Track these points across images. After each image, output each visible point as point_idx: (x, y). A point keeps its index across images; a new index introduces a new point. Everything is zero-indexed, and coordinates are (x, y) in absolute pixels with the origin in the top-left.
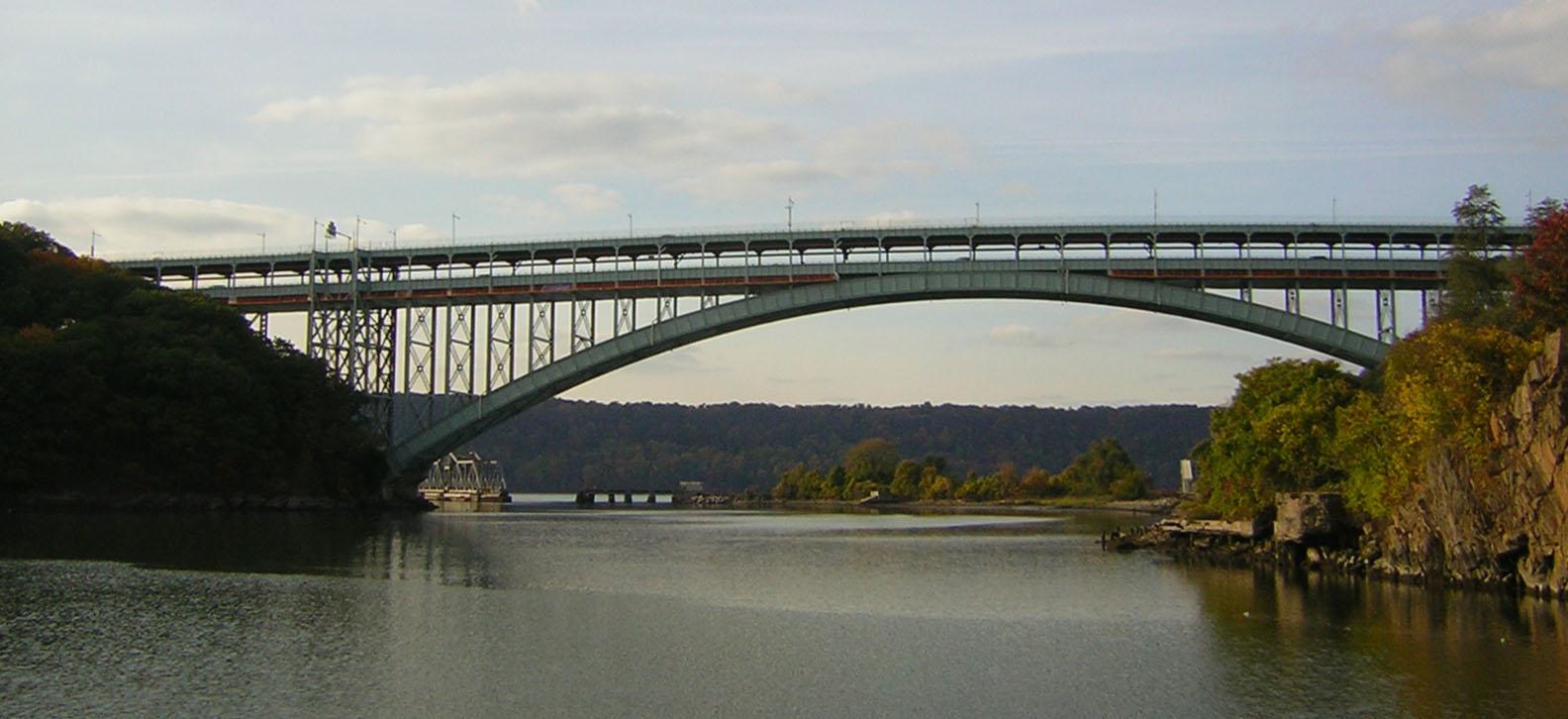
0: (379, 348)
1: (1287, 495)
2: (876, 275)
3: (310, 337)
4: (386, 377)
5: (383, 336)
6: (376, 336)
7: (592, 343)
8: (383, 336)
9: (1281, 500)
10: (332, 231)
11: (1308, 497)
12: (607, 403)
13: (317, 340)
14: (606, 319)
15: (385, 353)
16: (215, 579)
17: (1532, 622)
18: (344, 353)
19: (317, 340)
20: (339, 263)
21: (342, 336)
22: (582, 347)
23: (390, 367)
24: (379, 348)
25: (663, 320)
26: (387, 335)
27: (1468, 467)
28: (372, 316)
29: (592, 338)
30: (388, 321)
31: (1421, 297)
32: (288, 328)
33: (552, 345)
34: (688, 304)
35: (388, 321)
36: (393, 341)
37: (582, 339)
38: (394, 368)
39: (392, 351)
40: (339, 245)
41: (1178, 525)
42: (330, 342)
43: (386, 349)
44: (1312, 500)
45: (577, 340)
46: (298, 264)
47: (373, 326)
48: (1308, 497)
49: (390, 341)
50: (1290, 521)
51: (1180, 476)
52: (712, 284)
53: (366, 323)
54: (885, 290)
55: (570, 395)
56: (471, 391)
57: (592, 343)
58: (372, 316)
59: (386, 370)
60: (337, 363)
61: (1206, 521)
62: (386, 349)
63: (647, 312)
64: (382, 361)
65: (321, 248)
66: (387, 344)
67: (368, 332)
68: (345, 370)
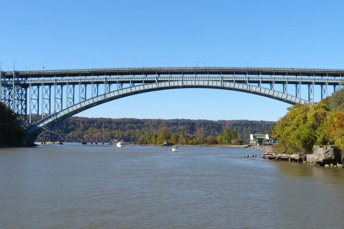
0: (22, 100)
1: (318, 146)
2: (168, 81)
4: (24, 109)
5: (23, 97)
6: (21, 97)
7: (86, 99)
8: (23, 97)
9: (316, 148)
11: (327, 147)
15: (24, 102)
18: (11, 102)
21: (23, 111)
23: (25, 106)
24: (22, 100)
26: (24, 97)
28: (20, 91)
29: (85, 98)
30: (24, 93)
31: (65, 110)
33: (74, 100)
35: (24, 93)
36: (26, 98)
38: (27, 106)
39: (26, 101)
41: (271, 155)
42: (7, 98)
43: (24, 101)
44: (328, 148)
47: (20, 94)
48: (327, 147)
49: (25, 99)
50: (319, 155)
51: (250, 139)
54: (145, 88)
55: (80, 115)
56: (38, 113)
57: (86, 99)
58: (20, 91)
59: (24, 107)
60: (9, 105)
61: (281, 154)
62: (24, 101)
64: (23, 104)
66: (24, 99)
67: (18, 96)
68: (11, 107)
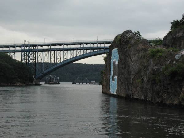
3: (22, 58)
10: (25, 41)
12: (91, 64)
13: (23, 59)
14: (76, 54)
16: (5, 89)
17: (118, 116)
19: (23, 59)
20: (26, 46)
22: (65, 60)
25: (71, 58)
27: (25, 102)
29: (67, 58)
32: (18, 57)
34: (89, 51)
36: (36, 59)
37: (65, 59)
40: (26, 43)
45: (64, 59)
46: (20, 46)
52: (93, 48)
53: (31, 56)
63: (82, 52)
65: (23, 44)
66: (35, 59)
